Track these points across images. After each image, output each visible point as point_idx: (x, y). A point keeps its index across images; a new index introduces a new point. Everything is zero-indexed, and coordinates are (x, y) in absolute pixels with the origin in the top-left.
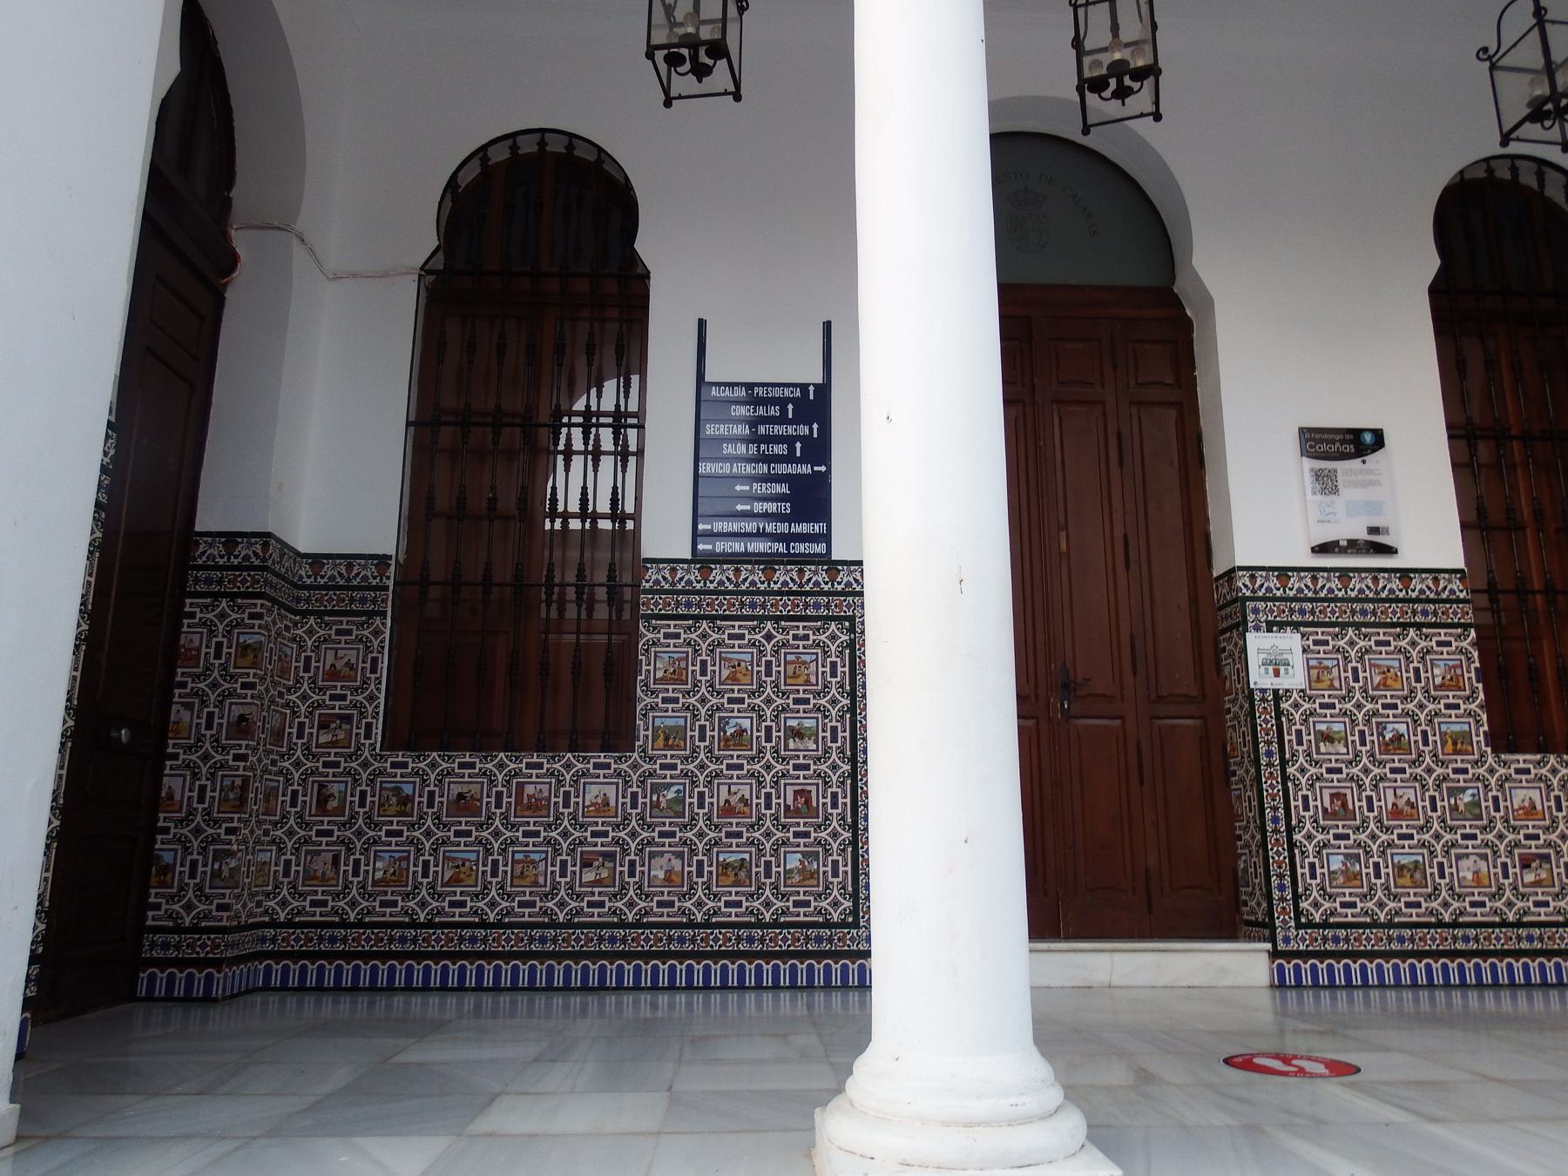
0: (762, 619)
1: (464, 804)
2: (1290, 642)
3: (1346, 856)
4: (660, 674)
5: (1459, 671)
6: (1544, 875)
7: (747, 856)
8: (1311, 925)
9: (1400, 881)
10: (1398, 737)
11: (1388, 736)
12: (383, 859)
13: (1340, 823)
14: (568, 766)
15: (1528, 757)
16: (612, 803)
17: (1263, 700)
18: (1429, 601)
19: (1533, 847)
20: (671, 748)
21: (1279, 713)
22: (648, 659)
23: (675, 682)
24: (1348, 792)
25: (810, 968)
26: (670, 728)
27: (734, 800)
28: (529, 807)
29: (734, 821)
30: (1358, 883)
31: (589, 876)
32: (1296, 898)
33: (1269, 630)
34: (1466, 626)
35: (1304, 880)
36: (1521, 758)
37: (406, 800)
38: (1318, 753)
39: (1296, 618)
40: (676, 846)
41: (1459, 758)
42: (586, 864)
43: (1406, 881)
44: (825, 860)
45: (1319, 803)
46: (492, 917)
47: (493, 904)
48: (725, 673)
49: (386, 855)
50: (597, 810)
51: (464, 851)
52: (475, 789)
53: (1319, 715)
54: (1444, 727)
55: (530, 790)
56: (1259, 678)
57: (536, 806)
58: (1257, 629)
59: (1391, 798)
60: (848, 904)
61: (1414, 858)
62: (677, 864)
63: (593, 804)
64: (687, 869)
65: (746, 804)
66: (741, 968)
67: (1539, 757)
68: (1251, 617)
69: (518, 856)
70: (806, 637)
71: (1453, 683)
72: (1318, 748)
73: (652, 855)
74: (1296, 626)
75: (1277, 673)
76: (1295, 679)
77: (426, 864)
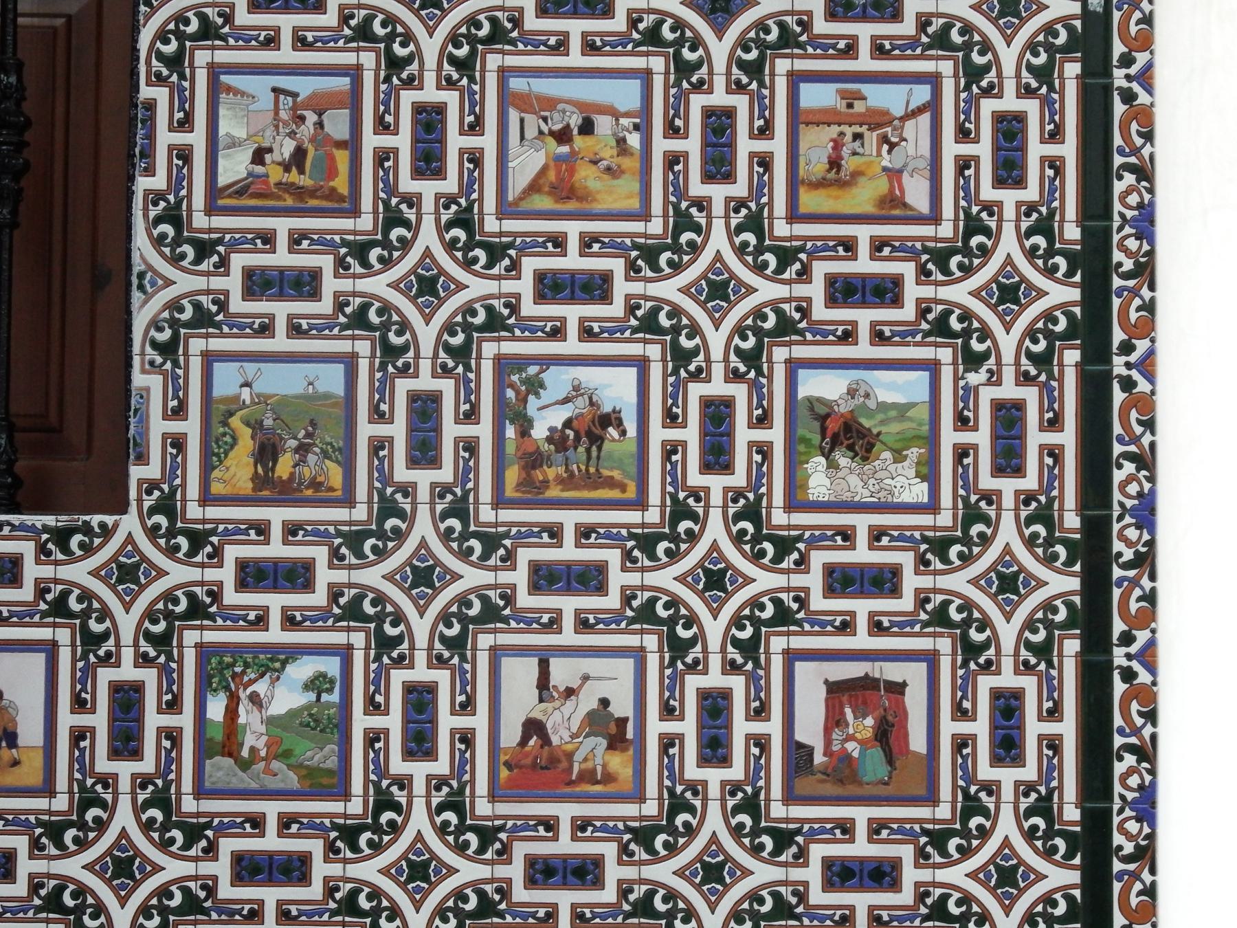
24: (914, 675)
27: (564, 723)
29: (565, 812)
45: (773, 727)
59: (519, 695)
65: (617, 741)
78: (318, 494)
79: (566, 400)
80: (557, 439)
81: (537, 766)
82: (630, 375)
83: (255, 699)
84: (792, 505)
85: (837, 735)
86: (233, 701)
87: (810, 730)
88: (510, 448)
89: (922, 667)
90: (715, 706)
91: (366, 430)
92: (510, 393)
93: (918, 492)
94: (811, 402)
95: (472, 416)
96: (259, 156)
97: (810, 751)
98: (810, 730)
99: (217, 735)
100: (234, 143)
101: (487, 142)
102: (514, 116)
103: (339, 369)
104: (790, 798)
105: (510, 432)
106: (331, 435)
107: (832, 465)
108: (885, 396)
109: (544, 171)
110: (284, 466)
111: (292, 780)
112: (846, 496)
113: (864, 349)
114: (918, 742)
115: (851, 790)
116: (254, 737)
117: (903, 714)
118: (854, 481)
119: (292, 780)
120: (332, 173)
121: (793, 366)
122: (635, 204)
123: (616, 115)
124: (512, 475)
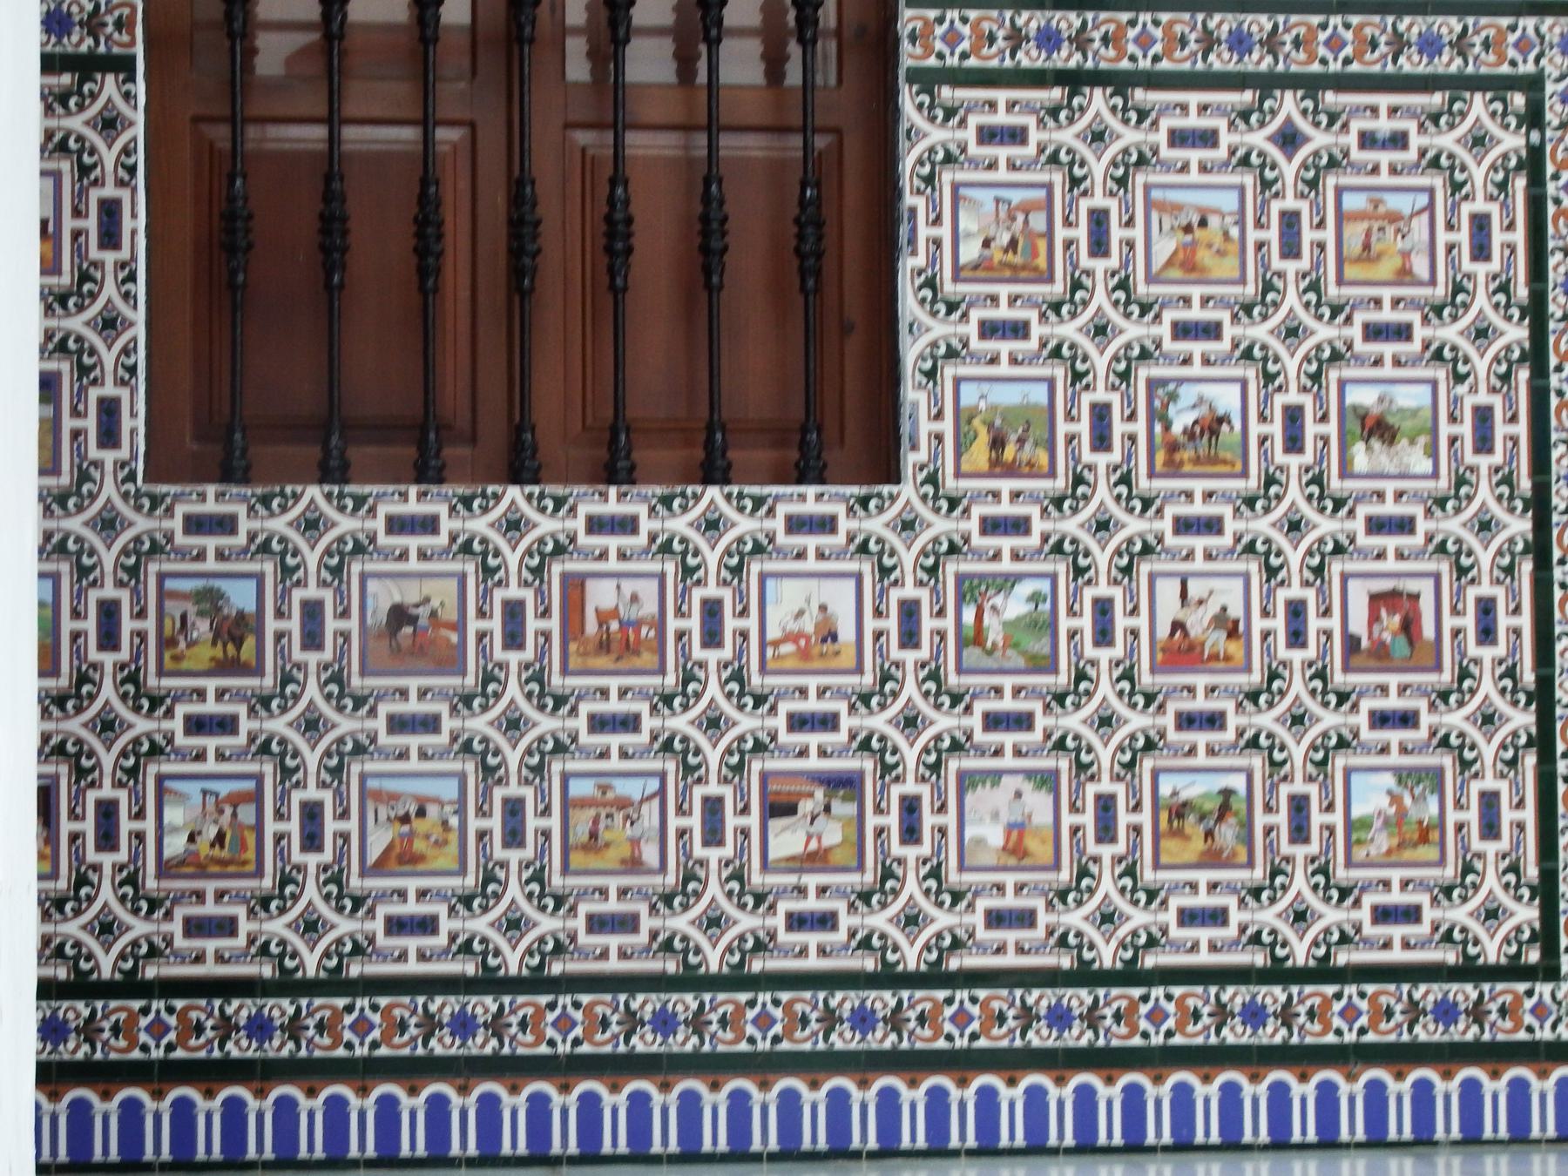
0: (1267, 84)
1: (406, 635)
3: (1402, 775)
4: (970, 251)
6: (832, 834)
7: (1238, 782)
10: (1213, 425)
11: (1182, 420)
12: (182, 797)
13: (1393, 680)
14: (712, 525)
16: (847, 633)
19: (817, 754)
20: (1011, 471)
22: (935, 206)
23: (1015, 274)
24: (1425, 588)
25: (1133, 1096)
26: (1008, 413)
27: (1198, 622)
28: (604, 646)
29: (1201, 681)
30: (1430, 853)
31: (788, 839)
38: (1345, 472)
40: (1035, 752)
41: (1006, 486)
45: (1334, 623)
46: (713, 960)
47: (311, 927)
48: (1164, 248)
49: (193, 789)
50: (804, 654)
51: (425, 774)
52: (442, 594)
54: (969, 395)
55: (601, 595)
57: (622, 644)
60: (1527, 914)
62: (1038, 805)
64: (1067, 820)
65: (1233, 633)
66: (1133, 1096)
67: (855, 490)
69: (579, 788)
70: (1398, 141)
73: (966, 781)
77: (312, 813)
78: (1032, 472)
80: (1190, 434)
81: (1181, 651)
82: (1236, 389)
83: (994, 608)
87: (1359, 625)
91: (1062, 428)
93: (1426, 466)
94: (1355, 408)
99: (971, 633)
102: (1155, 216)
105: (1158, 428)
106: (1039, 431)
107: (1369, 449)
109: (1175, 253)
110: (1009, 453)
112: (1378, 469)
113: (1388, 371)
114: (1428, 631)
116: (994, 634)
119: (1021, 662)
120: (1035, 254)
121: (1342, 384)
124: (1160, 457)
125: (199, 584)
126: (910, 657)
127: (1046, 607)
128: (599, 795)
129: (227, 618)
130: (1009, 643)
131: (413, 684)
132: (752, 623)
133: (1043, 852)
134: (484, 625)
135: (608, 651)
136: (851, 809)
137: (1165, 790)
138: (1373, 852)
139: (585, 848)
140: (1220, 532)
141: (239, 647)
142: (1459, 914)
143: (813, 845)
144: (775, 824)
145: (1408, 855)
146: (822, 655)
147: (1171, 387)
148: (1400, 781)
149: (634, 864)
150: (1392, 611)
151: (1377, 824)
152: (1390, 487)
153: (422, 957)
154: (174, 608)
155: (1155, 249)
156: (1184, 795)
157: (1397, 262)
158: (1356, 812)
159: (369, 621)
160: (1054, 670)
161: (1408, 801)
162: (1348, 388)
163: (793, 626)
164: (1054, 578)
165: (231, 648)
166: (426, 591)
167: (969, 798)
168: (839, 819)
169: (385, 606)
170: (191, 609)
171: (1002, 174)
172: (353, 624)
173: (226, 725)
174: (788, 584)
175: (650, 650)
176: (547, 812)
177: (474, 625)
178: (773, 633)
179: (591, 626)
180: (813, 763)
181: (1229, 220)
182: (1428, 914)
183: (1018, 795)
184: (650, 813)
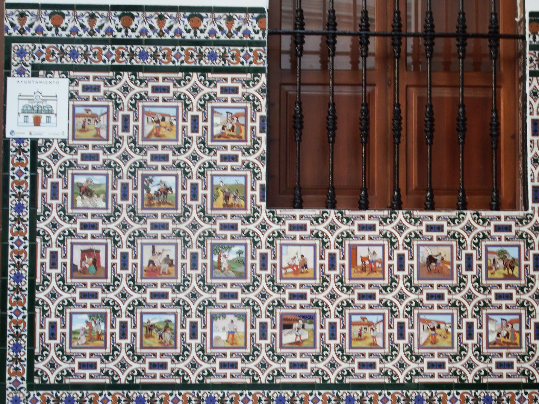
2: (57, 87)
3: (91, 315)
5: (242, 120)
6: (305, 335)
7: (172, 318)
8: (44, 386)
9: (148, 342)
10: (166, 191)
11: (154, 189)
13: (89, 281)
15: (443, 213)
16: (310, 265)
17: (20, 150)
18: (149, 42)
19: (298, 307)
21: (35, 164)
24: (102, 249)
27: (159, 261)
28: (363, 269)
29: (159, 282)
30: (102, 343)
31: (289, 337)
32: (32, 357)
33: (35, 75)
34: (256, 71)
35: (42, 341)
36: (436, 216)
37: (511, 264)
38: (73, 207)
39: (67, 61)
40: (238, 306)
41: (229, 213)
42: (287, 326)
43: (154, 341)
44: (113, 321)
45: (68, 261)
50: (296, 272)
52: (445, 252)
53: (80, 167)
55: (362, 252)
56: (17, 127)
57: (370, 268)
58: (21, 73)
59: (148, 255)
61: (164, 318)
62: (240, 325)
63: (290, 266)
64: (249, 331)
65: (171, 265)
68: (15, 60)
71: (233, 133)
72: (74, 201)
73: (214, 317)
74: (65, 69)
75: (37, 122)
76: (56, 128)
78: (239, 208)
79: (159, 184)
80: (157, 194)
81: (152, 271)
82: (174, 178)
83: (225, 256)
84: (73, 208)
85: (83, 263)
86: (220, 256)
87: (77, 261)
88: (145, 196)
89: (104, 247)
90: (401, 258)
91: (250, 193)
92: (145, 183)
93: (103, 205)
94: (77, 183)
95: (136, 188)
96: (223, 128)
97: (76, 266)
98: (77, 261)
99: (216, 265)
100: (218, 125)
101: (139, 123)
102: (146, 117)
103: (243, 178)
104: (72, 277)
105: (145, 192)
106: (241, 194)
107: (83, 198)
108: (95, 182)
109: (153, 131)
110: (231, 201)
111: (233, 275)
112: (86, 206)
113: (90, 171)
114: (103, 264)
115: (86, 276)
116: (225, 265)
117: (99, 257)
118: (88, 202)
119: (233, 275)
120: (241, 132)
121: (73, 175)
122: (175, 138)
123: (170, 116)
124: (146, 202)
125: (499, 249)
126: (469, 274)
127: (243, 256)
128: (361, 321)
129: (508, 260)
130: (230, 267)
131: (435, 283)
132: (277, 262)
133: (241, 342)
134: (391, 262)
135: (365, 271)
136: (311, 327)
137: (145, 321)
138: (80, 343)
139: (357, 339)
140: (442, 231)
141: (512, 270)
142: (389, 365)
143: (298, 339)
144: (285, 332)
145: (91, 344)
146: (302, 273)
147: (150, 177)
148: (90, 317)
149: (374, 345)
150: (89, 257)
151: (82, 333)
152: (89, 212)
153: (91, 377)
154: (491, 257)
155: (145, 128)
156: (152, 322)
157: (94, 132)
158: (74, 329)
159: (421, 261)
160: (246, 278)
161: (93, 325)
162: (75, 177)
163: (292, 263)
164: (246, 245)
165: (510, 271)
166: (439, 251)
167: (215, 323)
168: (307, 330)
169: (426, 256)
170: (496, 257)
171: (229, 104)
172: (415, 262)
173: (164, 296)
174: (290, 248)
175: (380, 271)
176: (135, 327)
177: (456, 262)
178: (285, 265)
179: (359, 263)
180: (298, 310)
181: (172, 118)
182: (76, 366)
183: (232, 321)
184: (379, 328)
